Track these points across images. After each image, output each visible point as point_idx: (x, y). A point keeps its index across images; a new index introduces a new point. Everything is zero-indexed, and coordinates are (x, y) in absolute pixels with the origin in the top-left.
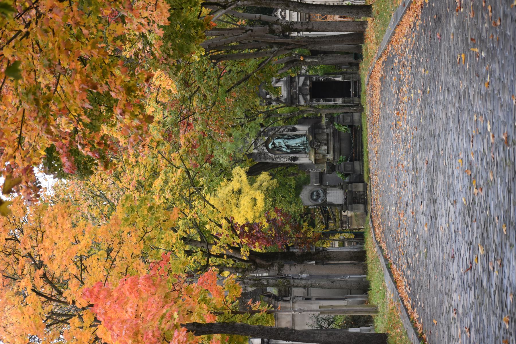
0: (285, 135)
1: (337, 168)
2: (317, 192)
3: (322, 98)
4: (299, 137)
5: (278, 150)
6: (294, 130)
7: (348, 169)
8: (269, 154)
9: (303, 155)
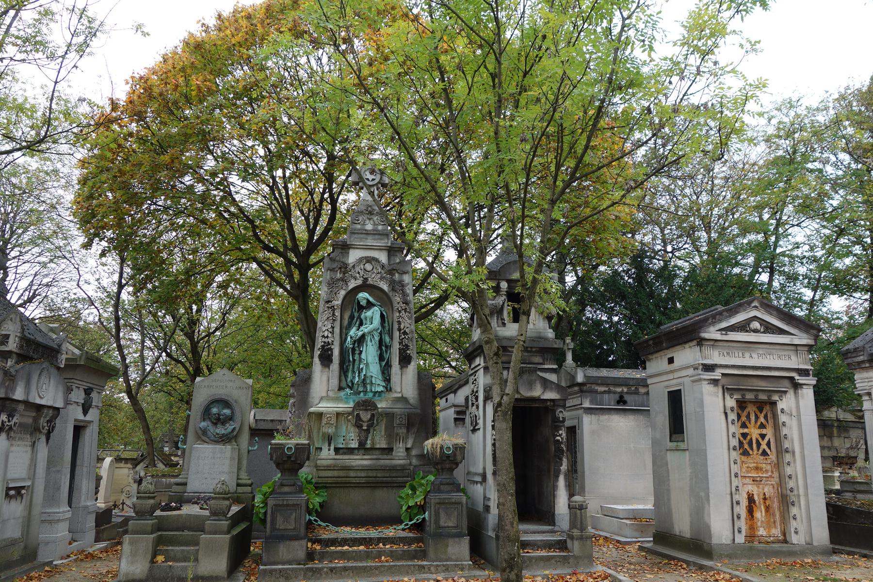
0: (392, 338)
2: (231, 418)
4: (383, 373)
5: (352, 317)
7: (280, 520)
8: (343, 293)
9: (335, 382)
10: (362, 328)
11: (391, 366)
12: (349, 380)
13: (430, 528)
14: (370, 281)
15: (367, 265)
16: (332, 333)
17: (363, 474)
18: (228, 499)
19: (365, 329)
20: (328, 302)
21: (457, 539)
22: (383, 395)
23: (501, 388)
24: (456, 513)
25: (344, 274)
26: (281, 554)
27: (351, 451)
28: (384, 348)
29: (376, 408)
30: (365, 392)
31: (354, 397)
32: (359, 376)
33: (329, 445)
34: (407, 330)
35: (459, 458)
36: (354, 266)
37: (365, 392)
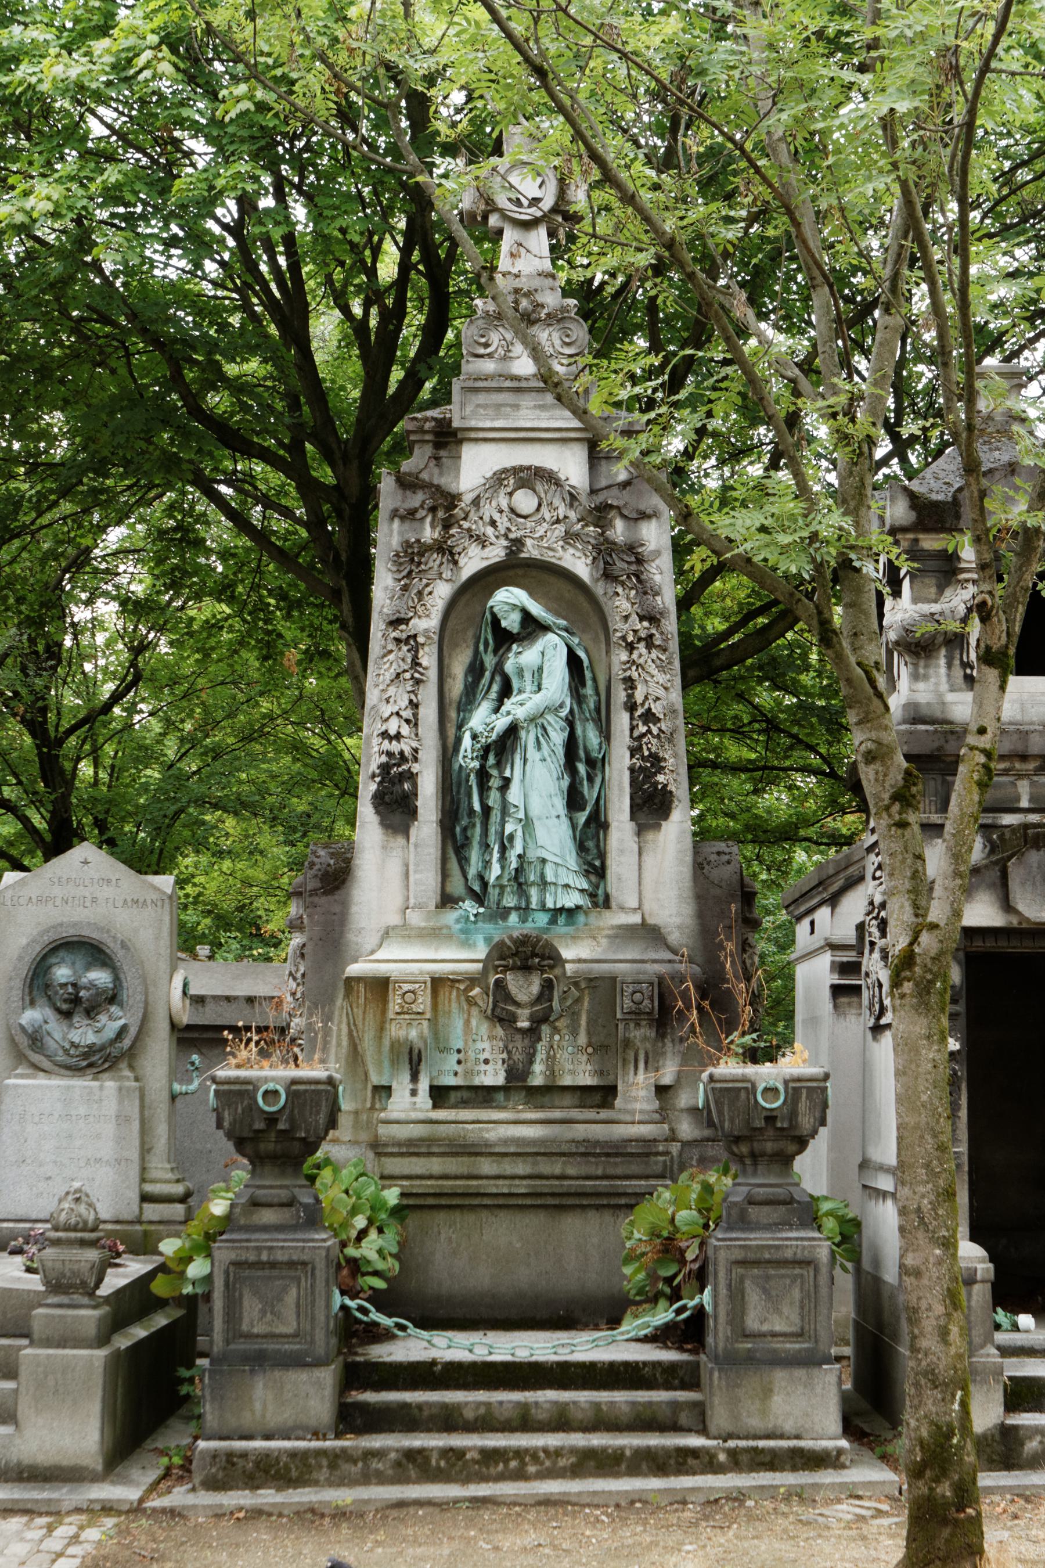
0: (606, 734)
1: (276, 1185)
2: (113, 997)
3: (971, 1043)
4: (581, 848)
5: (476, 670)
6: (651, 805)
7: (251, 1308)
8: (442, 592)
9: (427, 880)
10: (508, 705)
11: (605, 826)
12: (472, 872)
13: (718, 1335)
14: (531, 550)
15: (519, 494)
16: (413, 722)
17: (521, 1168)
18: (93, 1244)
19: (517, 708)
20: (396, 622)
21: (800, 1373)
22: (581, 918)
23: (916, 906)
24: (796, 1293)
25: (447, 526)
26: (258, 1406)
27: (482, 1096)
28: (582, 768)
29: (555, 959)
30: (524, 911)
31: (488, 927)
32: (503, 858)
33: (415, 1078)
34: (657, 709)
35: (806, 1122)
36: (476, 502)
37: (524, 911)
